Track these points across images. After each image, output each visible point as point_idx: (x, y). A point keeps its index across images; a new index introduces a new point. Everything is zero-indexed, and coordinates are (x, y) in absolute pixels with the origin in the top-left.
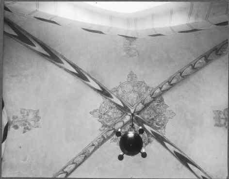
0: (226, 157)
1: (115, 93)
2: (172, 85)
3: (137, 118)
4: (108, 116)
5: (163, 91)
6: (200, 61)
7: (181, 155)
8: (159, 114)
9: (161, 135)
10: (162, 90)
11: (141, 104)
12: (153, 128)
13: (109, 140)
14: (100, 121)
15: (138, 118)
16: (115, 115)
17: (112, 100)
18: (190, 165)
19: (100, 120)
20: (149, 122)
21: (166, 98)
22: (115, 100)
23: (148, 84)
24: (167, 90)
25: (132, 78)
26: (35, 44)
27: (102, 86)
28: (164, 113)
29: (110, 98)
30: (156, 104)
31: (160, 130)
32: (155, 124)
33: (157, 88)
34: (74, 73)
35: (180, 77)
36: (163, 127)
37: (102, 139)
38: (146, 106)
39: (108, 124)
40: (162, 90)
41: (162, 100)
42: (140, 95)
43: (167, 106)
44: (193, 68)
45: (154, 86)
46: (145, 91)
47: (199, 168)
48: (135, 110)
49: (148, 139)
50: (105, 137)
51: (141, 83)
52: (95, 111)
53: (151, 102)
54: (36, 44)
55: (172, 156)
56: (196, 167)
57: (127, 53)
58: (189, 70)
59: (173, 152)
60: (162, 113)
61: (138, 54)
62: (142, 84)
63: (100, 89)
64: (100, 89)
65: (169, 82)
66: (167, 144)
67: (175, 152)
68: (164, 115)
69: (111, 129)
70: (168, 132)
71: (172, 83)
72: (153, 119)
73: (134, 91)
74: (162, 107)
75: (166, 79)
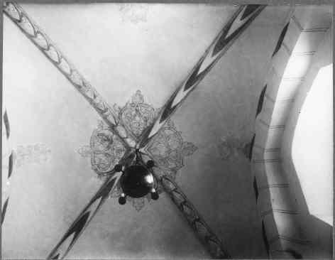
1: (166, 126)
4: (135, 116)
6: (219, 249)
7: (85, 221)
13: (100, 118)
14: (127, 104)
16: (135, 125)
17: (158, 122)
18: (201, 71)
19: (128, 105)
22: (158, 126)
24: (173, 199)
39: (123, 116)
42: (164, 160)
44: (207, 239)
50: (106, 113)
51: (181, 161)
52: (141, 98)
59: (88, 211)
62: (179, 162)
63: (173, 105)
66: (99, 201)
67: (88, 213)
73: (169, 151)
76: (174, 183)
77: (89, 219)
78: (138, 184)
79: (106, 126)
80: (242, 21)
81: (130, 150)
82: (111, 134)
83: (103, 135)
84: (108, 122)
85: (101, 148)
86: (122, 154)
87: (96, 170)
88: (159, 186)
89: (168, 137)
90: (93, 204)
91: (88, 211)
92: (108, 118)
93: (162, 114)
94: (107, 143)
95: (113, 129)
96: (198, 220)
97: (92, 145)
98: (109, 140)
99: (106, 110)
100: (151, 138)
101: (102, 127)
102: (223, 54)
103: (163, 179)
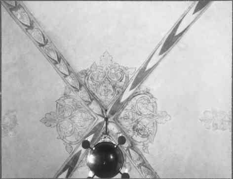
0: (231, 69)
1: (74, 147)
2: (59, 59)
3: (112, 113)
5: (70, 72)
6: (19, 17)
7: (165, 44)
8: (107, 78)
9: (136, 75)
10: (67, 73)
11: (90, 106)
12: (127, 86)
13: (145, 155)
15: (111, 110)
18: (178, 32)
20: (118, 93)
21: (80, 66)
23: (60, 94)
24: (68, 65)
25: (51, 120)
26: (133, 90)
27: (62, 169)
28: (104, 69)
29: (80, 156)
30: (90, 82)
31: (130, 76)
32: (121, 84)
33: (66, 82)
34: (176, 31)
35: (47, 46)
36: (125, 71)
37: (142, 167)
38: (93, 97)
40: (67, 73)
41: (85, 73)
42: (77, 107)
43: (94, 65)
44: (31, 27)
45: (63, 85)
46: (71, 100)
47: (184, 16)
48: (100, 115)
49: (144, 94)
50: (139, 162)
51: (58, 105)
53: (88, 91)
54: (158, 59)
55: (167, 57)
56: (180, 22)
57: (11, 129)
58: (35, 33)
60: (105, 72)
61: (12, 112)
62: (60, 105)
63: (67, 171)
64: (67, 171)
65: (56, 63)
66: (149, 66)
67: (160, 54)
68: (107, 69)
69: (128, 152)
70: (134, 66)
71: (56, 59)
72: (114, 87)
73: (71, 117)
74: (95, 72)
75: (51, 66)
76: (67, 83)
77: (161, 47)
78: (115, 146)
79: (140, 147)
80: (193, 15)
81: (114, 119)
82: (134, 137)
83: (143, 136)
84: (137, 151)
85: (145, 121)
86: (123, 114)
87: (152, 97)
88: (83, 79)
89: (72, 133)
90: (156, 62)
91: (161, 56)
92: (138, 156)
93: (79, 161)
94: (139, 127)
95: (140, 155)
96: (41, 45)
97: (155, 124)
98: (137, 130)
99: (139, 166)
100: (181, 34)
101: (144, 145)
102: (201, 14)
103: (78, 87)
